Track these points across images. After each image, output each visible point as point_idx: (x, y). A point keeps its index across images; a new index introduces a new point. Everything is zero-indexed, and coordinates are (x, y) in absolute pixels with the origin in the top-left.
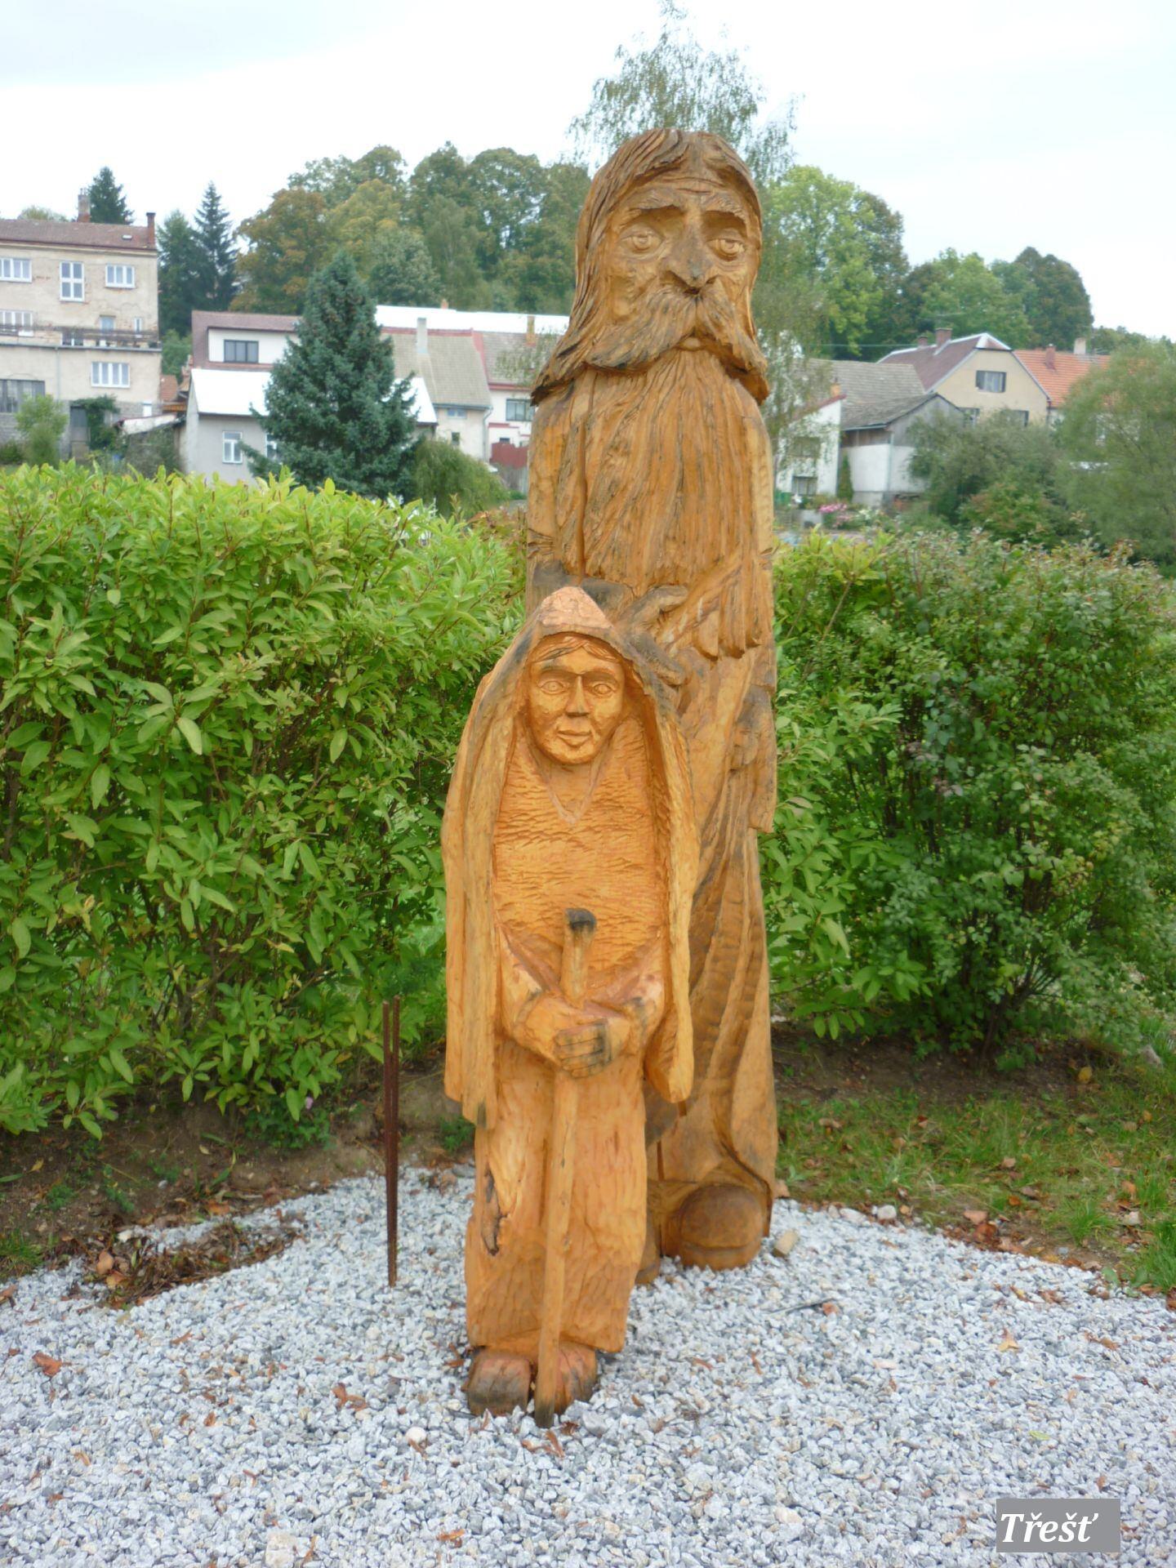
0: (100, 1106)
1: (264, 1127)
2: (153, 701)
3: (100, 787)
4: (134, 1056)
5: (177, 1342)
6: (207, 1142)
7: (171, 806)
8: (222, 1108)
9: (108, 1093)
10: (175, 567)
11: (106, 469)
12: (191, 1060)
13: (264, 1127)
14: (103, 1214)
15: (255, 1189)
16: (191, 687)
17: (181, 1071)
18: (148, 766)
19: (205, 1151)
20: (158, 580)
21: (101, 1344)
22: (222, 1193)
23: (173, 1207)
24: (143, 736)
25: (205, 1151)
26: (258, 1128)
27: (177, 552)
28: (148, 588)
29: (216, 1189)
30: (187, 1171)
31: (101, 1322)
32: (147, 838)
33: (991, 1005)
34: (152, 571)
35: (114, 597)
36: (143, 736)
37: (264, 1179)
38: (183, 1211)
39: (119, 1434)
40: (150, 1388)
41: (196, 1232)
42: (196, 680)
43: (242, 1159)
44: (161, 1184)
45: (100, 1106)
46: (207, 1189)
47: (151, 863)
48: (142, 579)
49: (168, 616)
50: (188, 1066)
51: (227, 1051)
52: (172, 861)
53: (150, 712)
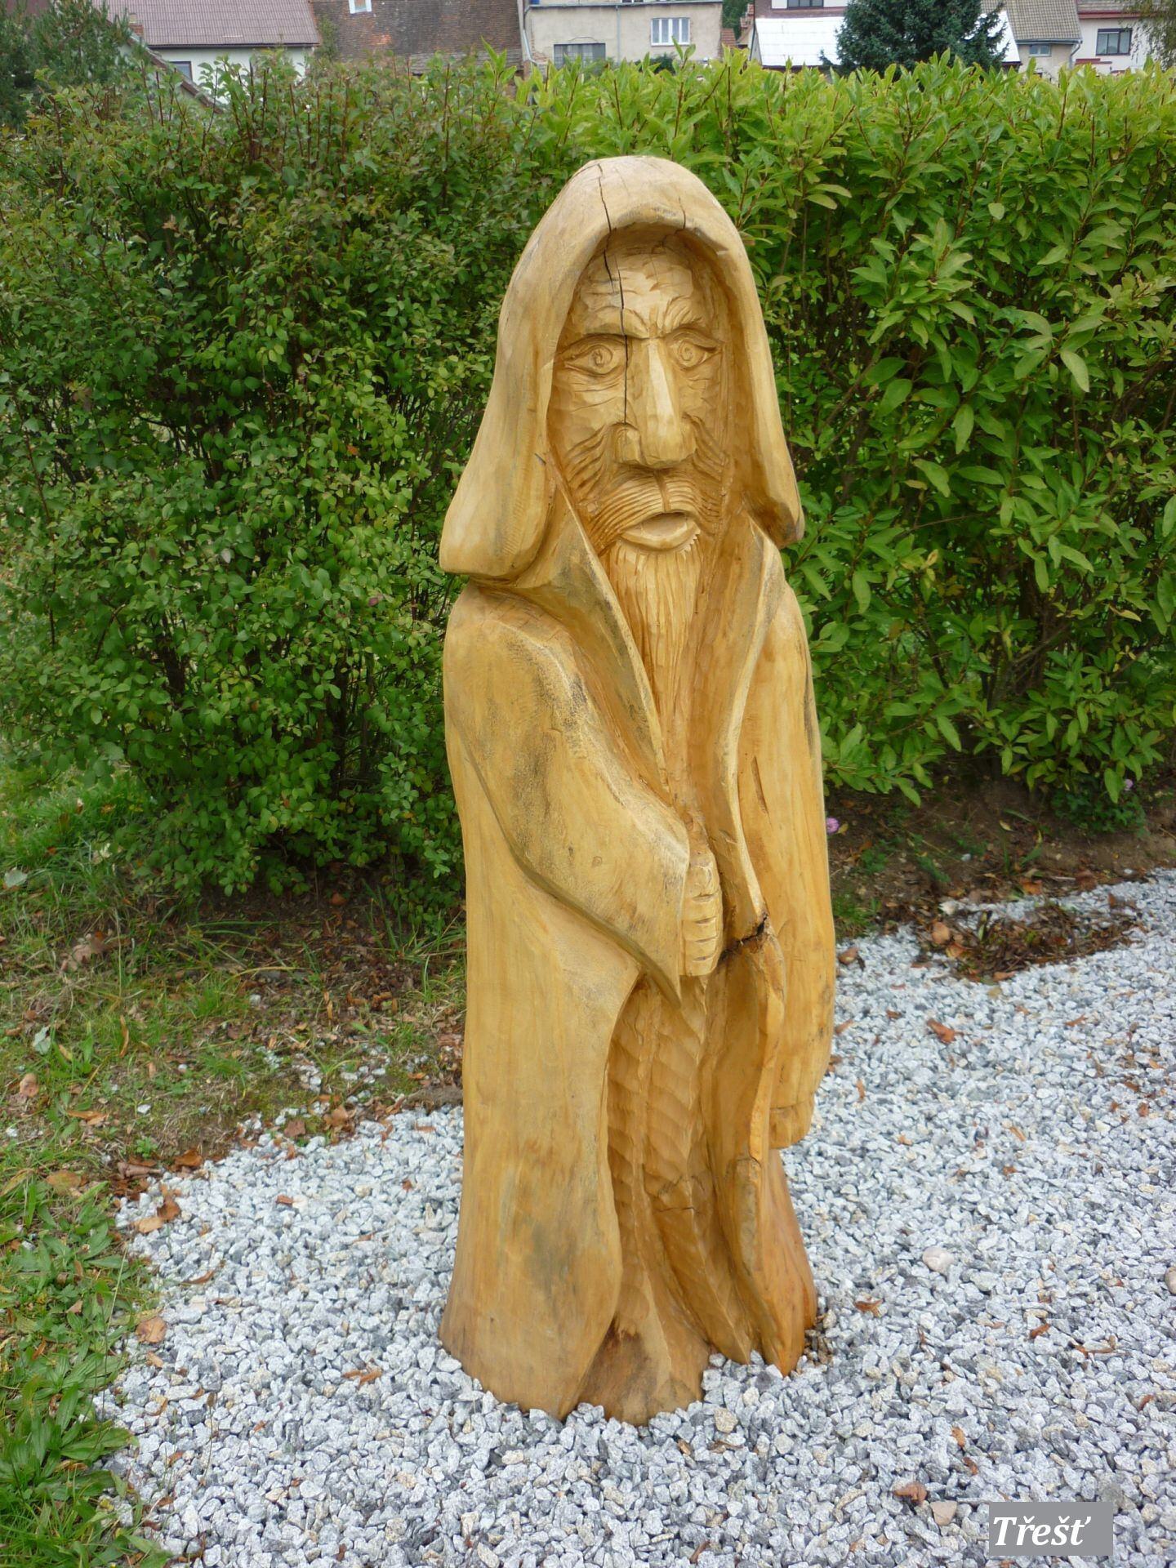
0: (919, 772)
1: (1074, 807)
2: (1031, 334)
3: (963, 427)
4: (962, 723)
5: (1072, 1024)
6: (1010, 819)
7: (1030, 453)
8: (1031, 784)
9: (925, 760)
10: (1066, 173)
11: (564, 130)
12: (1010, 731)
13: (1074, 807)
14: (919, 883)
15: (1063, 871)
16: (1072, 319)
17: (998, 742)
18: (1012, 409)
19: (1006, 827)
20: (1045, 191)
21: (980, 1016)
22: (1032, 872)
23: (982, 882)
24: (1021, 371)
25: (1006, 827)
26: (1066, 807)
27: (1068, 156)
28: (1032, 200)
29: (1026, 868)
30: (990, 847)
31: (978, 993)
32: (1000, 487)
33: (198, 725)
34: (1042, 179)
35: (997, 211)
36: (1021, 371)
37: (1072, 861)
38: (994, 887)
39: (1048, 1113)
40: (1064, 1069)
41: (1018, 909)
42: (1076, 308)
43: (1048, 839)
44: (966, 857)
45: (919, 772)
46: (1017, 867)
47: (1005, 515)
48: (1028, 189)
49: (1051, 234)
50: (1010, 740)
51: (1052, 724)
52: (1029, 516)
53: (1031, 344)
